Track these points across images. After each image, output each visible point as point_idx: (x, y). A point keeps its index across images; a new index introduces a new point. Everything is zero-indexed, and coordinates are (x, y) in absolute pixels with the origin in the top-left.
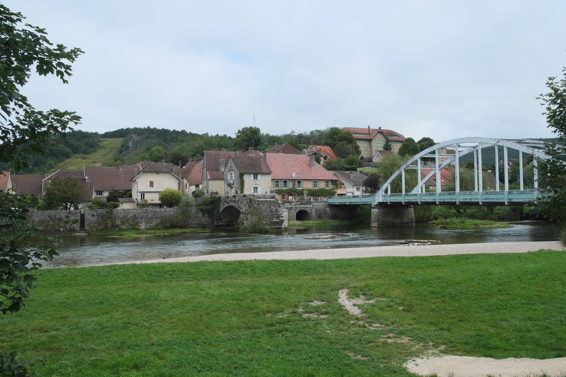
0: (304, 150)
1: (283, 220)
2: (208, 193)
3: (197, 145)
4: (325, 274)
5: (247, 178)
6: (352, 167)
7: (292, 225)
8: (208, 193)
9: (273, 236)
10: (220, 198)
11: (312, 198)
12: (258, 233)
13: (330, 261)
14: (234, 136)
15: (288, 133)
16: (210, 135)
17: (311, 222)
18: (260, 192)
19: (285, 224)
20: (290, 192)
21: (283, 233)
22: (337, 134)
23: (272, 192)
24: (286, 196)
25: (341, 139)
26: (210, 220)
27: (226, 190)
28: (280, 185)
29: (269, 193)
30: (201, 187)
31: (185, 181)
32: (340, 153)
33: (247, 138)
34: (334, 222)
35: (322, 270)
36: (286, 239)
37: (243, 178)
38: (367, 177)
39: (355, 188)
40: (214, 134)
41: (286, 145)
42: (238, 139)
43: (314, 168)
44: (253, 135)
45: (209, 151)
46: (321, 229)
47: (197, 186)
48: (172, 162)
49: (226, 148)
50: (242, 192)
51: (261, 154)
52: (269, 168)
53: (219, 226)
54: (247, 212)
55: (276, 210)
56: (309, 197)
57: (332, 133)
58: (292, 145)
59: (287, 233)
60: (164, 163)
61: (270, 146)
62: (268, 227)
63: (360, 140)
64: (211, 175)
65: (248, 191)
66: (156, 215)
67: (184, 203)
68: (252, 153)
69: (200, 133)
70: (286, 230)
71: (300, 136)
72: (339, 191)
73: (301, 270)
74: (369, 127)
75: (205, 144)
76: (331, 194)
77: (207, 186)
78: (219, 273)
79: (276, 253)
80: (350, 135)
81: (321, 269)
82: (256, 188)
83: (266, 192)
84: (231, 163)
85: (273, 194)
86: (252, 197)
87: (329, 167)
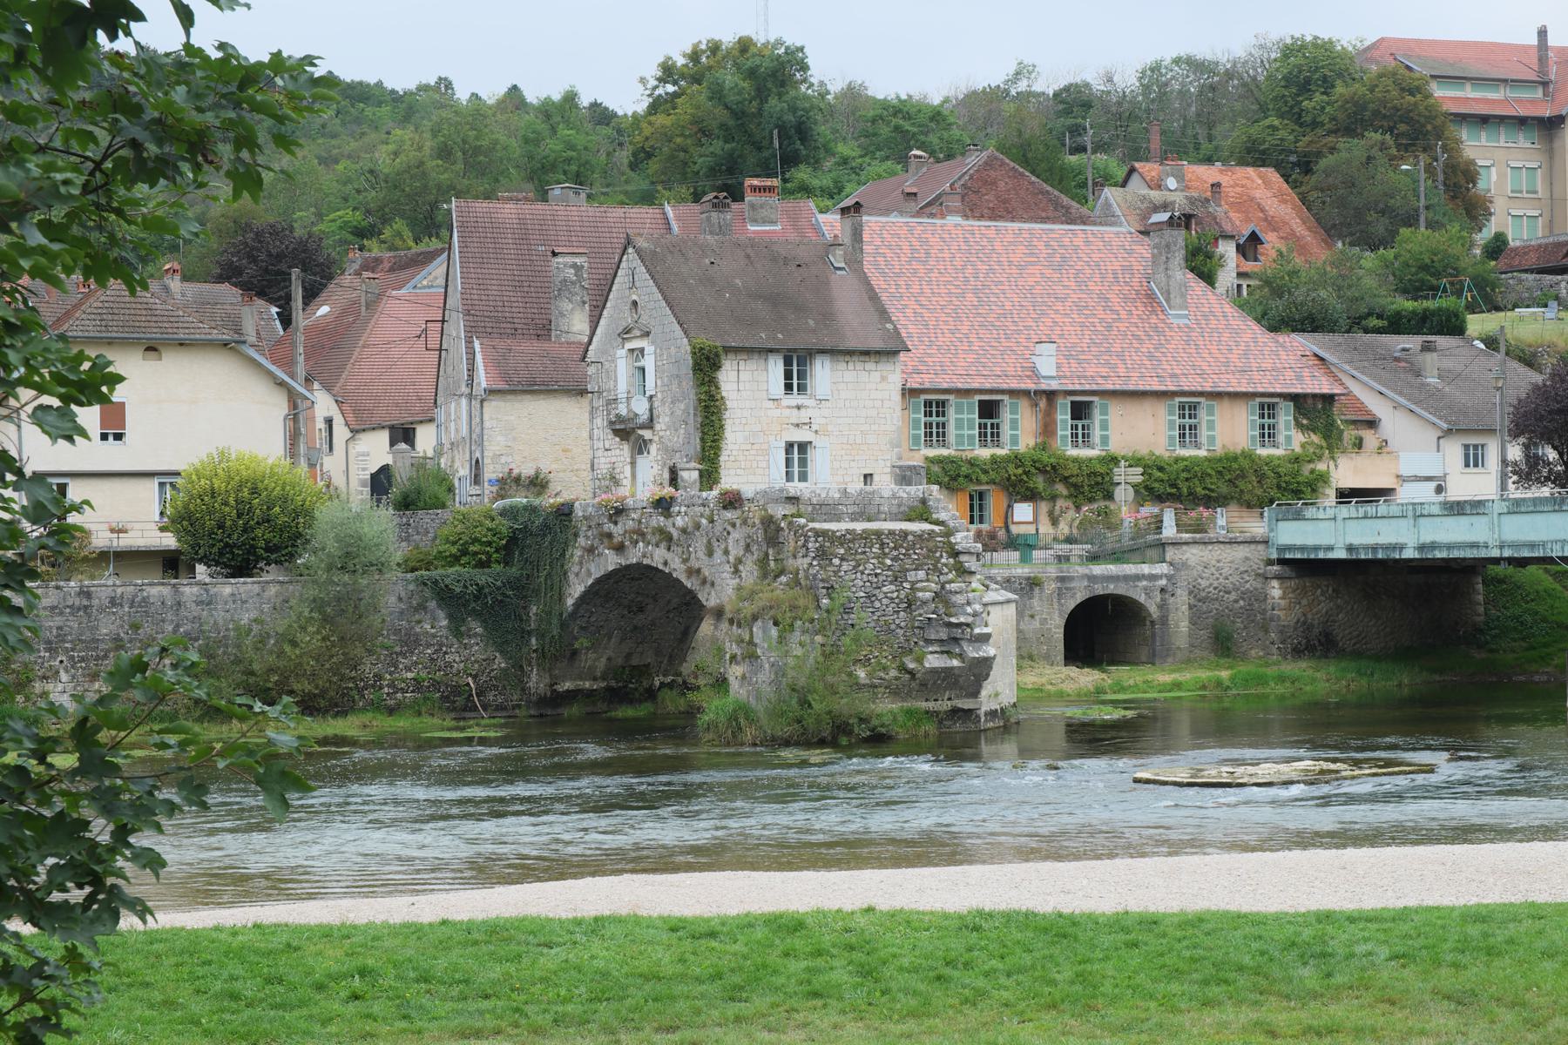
0: (1110, 194)
1: (985, 665)
2: (477, 479)
3: (383, 159)
4: (1336, 999)
5: (735, 380)
6: (1430, 305)
7: (1039, 695)
8: (477, 479)
9: (923, 766)
10: (564, 512)
11: (1169, 518)
12: (822, 743)
13: (1352, 919)
14: (628, 100)
15: (990, 73)
16: (462, 94)
17: (1165, 678)
18: (829, 476)
19: (1000, 690)
20: (1021, 480)
21: (985, 748)
22: (1327, 85)
23: (905, 476)
24: (995, 502)
25: (1355, 121)
26: (500, 663)
27: (603, 465)
28: (952, 431)
29: (885, 485)
30: (426, 439)
31: (323, 404)
32: (1351, 218)
33: (720, 112)
34: (1319, 679)
35: (1308, 975)
36: (1002, 791)
37: (713, 382)
38: (1538, 378)
39: (1454, 451)
40: (492, 91)
41: (988, 164)
42: (661, 119)
43: (1177, 317)
44: (761, 94)
45: (482, 206)
46: (1223, 724)
47: (403, 434)
48: (229, 274)
49: (579, 179)
50: (709, 477)
51: (831, 223)
52: (884, 314)
53: (558, 699)
54: (748, 609)
55: (941, 596)
56: (1149, 510)
57: (1288, 80)
58: (1025, 162)
59: (1010, 747)
60: (175, 284)
61: (877, 167)
62: (886, 708)
63: (1483, 120)
64: (498, 364)
65: (751, 466)
66: (147, 629)
67: (332, 547)
68: (766, 218)
69: (401, 80)
70: (1006, 724)
71: (1074, 102)
72: (1347, 472)
73: (1176, 974)
74: (1542, 33)
75: (444, 153)
76: (1291, 488)
77: (477, 438)
78: (660, 988)
79: (974, 871)
80: (1415, 89)
81: (1306, 972)
82: (803, 447)
83: (868, 478)
84: (634, 284)
85: (916, 491)
86: (779, 511)
87: (1284, 311)
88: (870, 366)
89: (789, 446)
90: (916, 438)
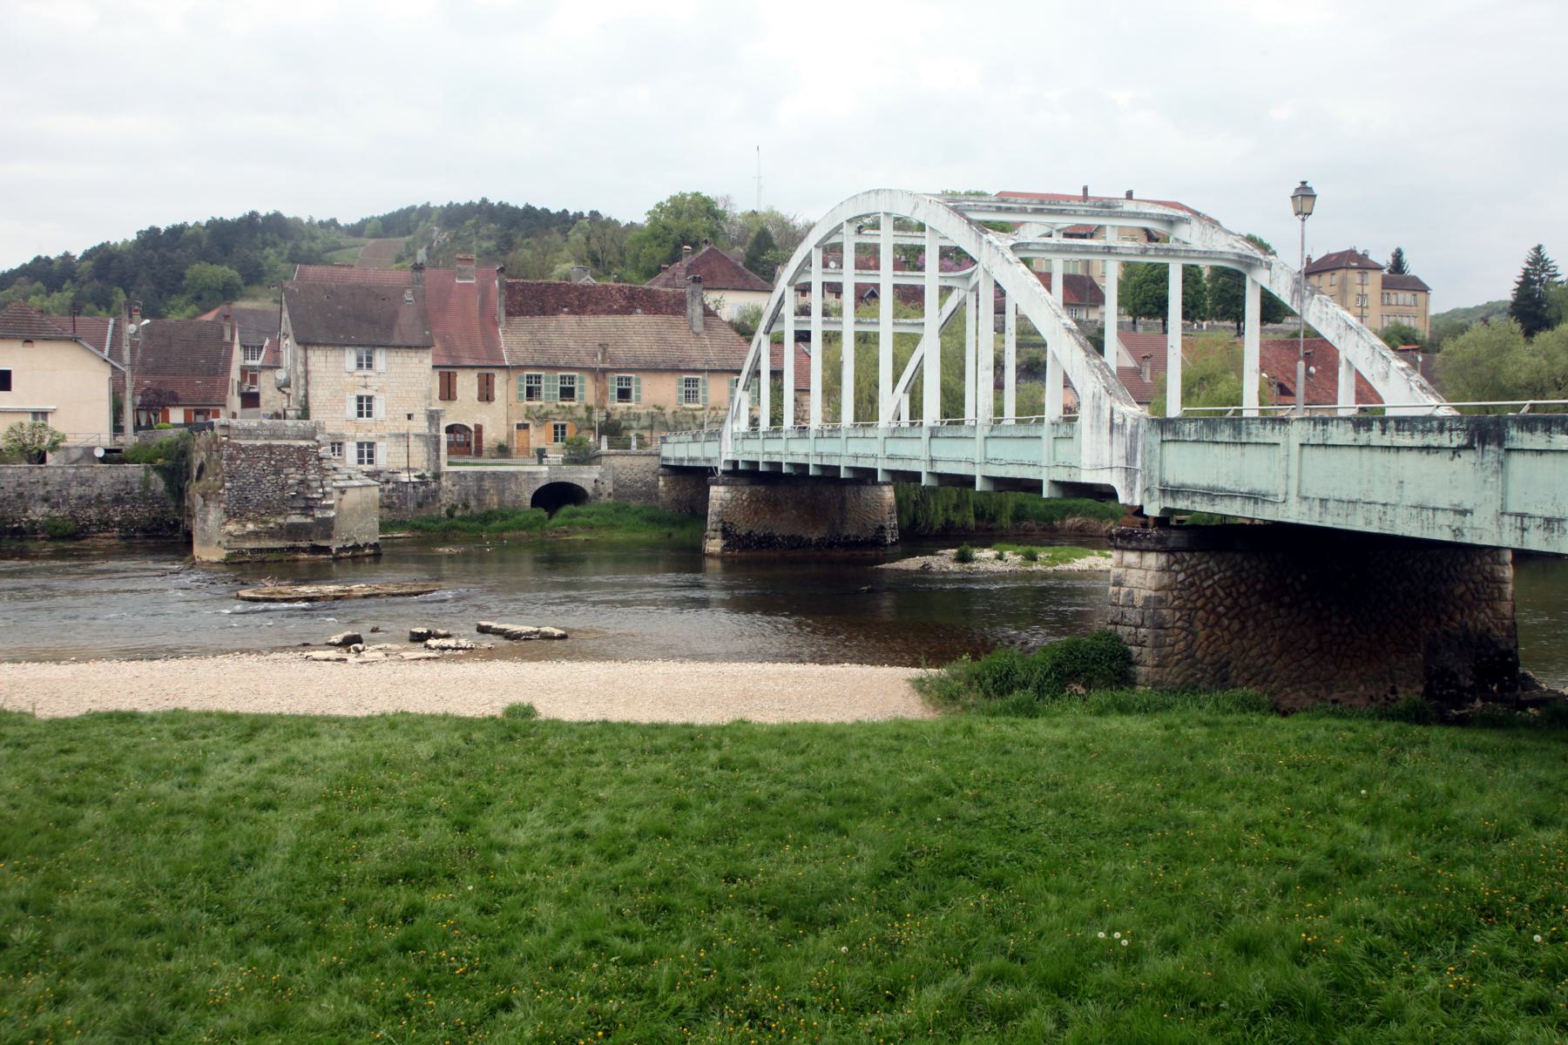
74: (1085, 189)
88: (412, 354)
89: (360, 399)
90: (521, 396)
